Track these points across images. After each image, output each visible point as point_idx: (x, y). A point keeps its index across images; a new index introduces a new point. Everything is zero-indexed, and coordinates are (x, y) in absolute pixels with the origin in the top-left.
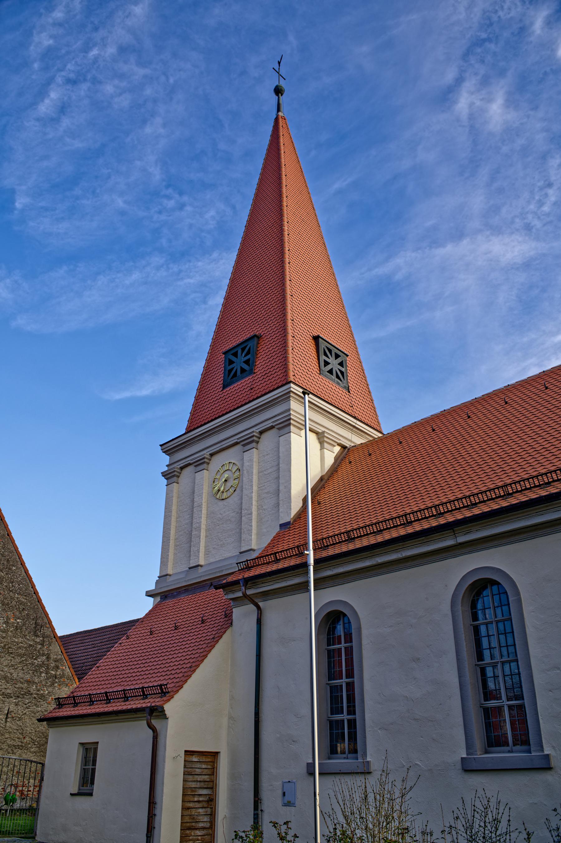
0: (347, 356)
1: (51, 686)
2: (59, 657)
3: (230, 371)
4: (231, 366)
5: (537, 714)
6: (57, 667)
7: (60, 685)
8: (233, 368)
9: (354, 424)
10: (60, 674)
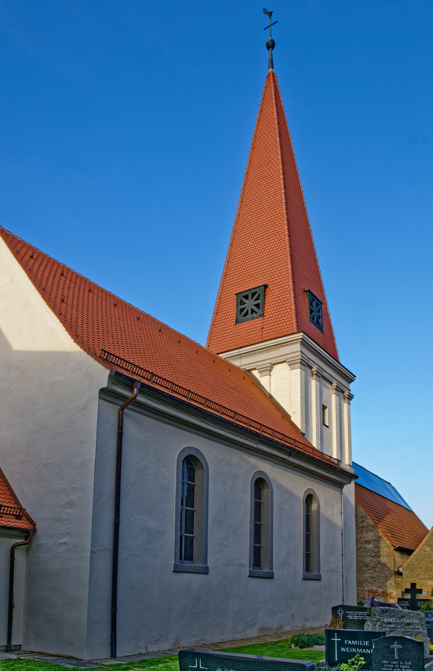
2: (364, 515)
3: (242, 310)
4: (243, 306)
6: (364, 521)
7: (367, 532)
8: (244, 308)
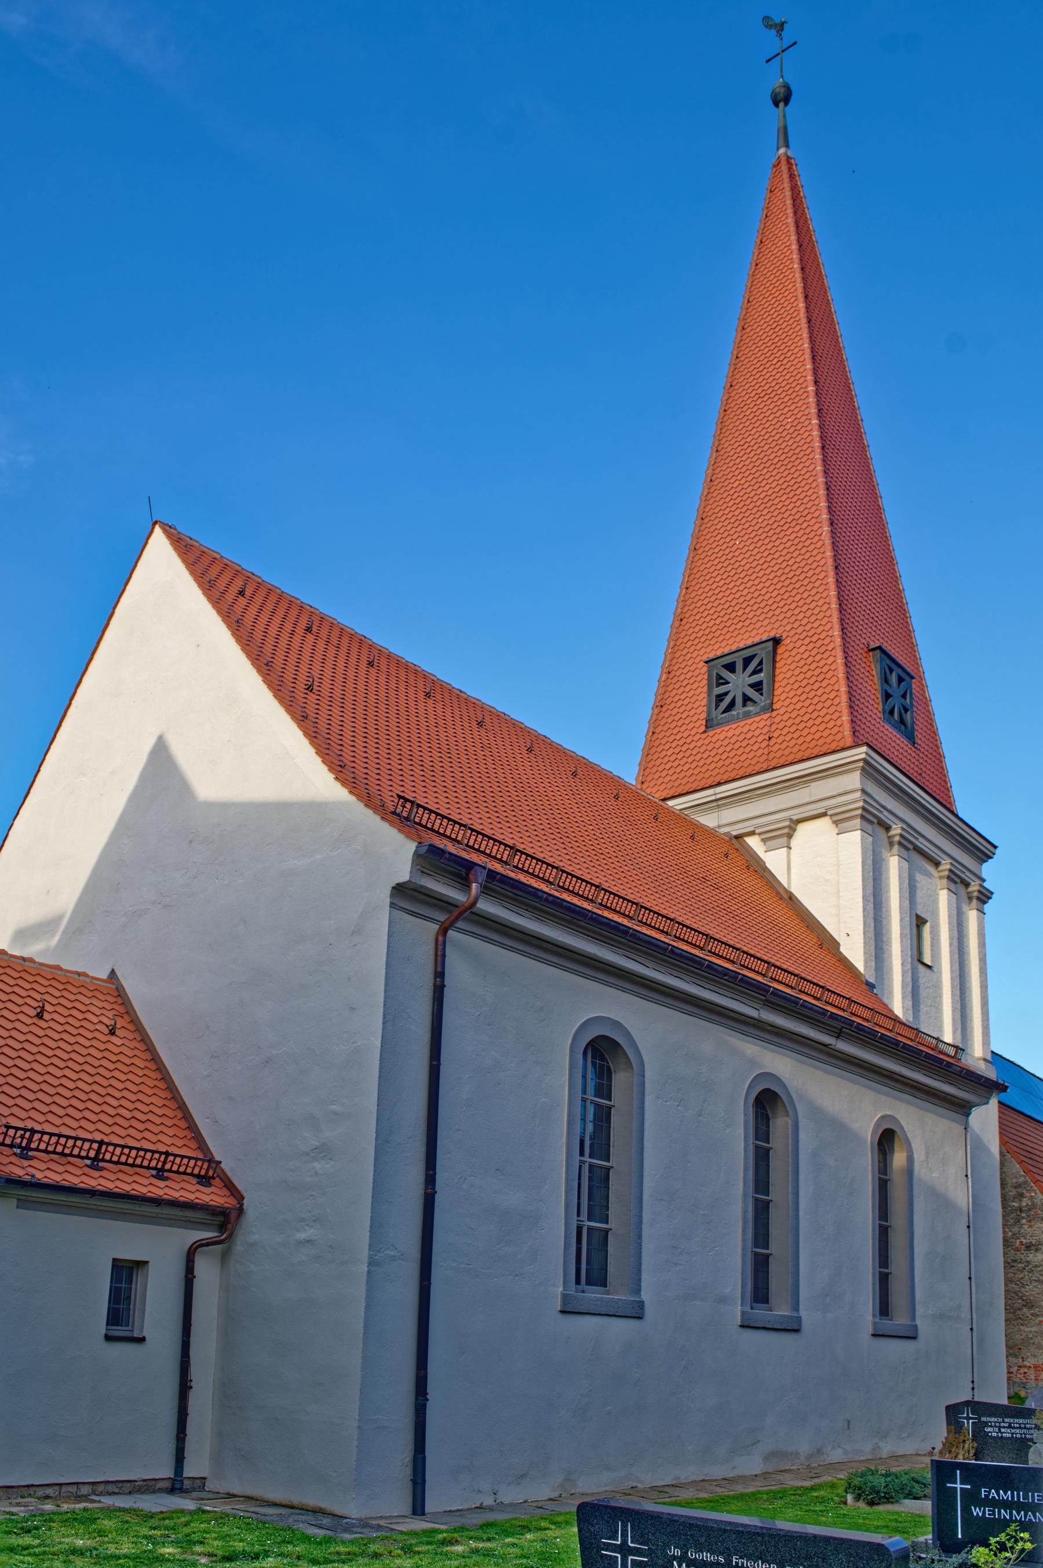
0: (912, 678)
1: (1015, 1224)
2: (1021, 1180)
3: (720, 698)
5: (565, 1256)
6: (1022, 1195)
7: (1030, 1221)
8: (726, 694)
9: (713, 798)
10: (1027, 1205)
